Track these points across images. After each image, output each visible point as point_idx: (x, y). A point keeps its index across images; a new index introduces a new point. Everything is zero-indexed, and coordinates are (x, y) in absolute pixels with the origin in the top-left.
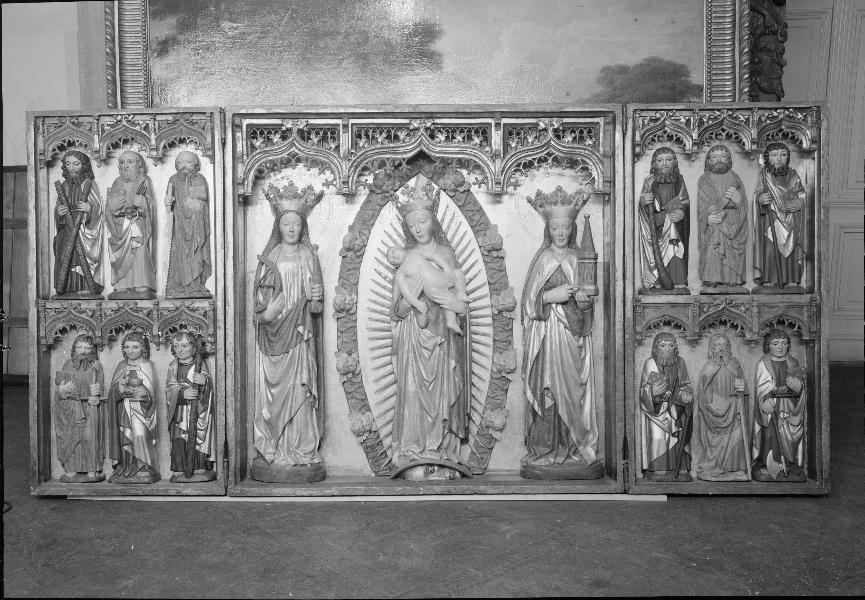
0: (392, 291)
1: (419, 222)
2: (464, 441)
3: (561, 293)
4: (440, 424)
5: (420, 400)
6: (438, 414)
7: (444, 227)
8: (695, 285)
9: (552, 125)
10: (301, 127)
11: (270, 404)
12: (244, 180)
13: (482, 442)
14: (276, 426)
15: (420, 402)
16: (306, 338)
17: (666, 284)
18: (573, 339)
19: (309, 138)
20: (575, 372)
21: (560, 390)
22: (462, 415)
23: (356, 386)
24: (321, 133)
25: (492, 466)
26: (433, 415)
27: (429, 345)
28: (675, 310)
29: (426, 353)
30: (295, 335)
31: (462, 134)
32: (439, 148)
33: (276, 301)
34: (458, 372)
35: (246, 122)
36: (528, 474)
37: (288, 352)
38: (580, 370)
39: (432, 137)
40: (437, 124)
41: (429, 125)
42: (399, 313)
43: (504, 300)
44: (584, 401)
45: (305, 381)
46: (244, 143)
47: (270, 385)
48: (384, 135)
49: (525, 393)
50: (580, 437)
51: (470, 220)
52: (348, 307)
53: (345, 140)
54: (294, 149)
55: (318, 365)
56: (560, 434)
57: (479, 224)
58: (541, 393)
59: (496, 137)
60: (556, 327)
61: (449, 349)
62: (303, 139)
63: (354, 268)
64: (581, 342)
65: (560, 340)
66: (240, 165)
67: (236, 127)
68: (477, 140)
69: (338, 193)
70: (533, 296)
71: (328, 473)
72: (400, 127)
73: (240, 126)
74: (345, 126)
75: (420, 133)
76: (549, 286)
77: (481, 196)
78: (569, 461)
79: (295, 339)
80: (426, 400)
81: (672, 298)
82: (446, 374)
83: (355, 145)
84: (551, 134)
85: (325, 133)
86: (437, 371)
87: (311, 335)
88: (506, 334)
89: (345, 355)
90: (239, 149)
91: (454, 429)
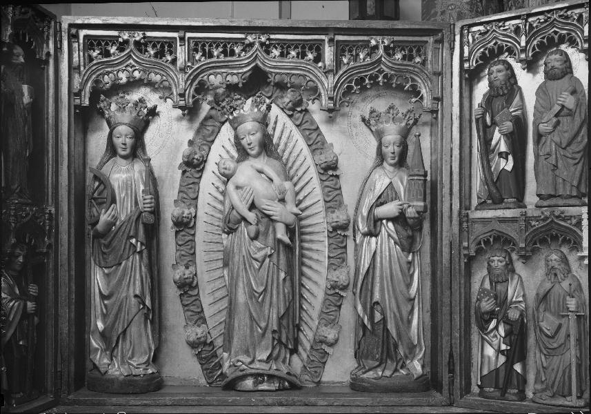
0: (222, 203)
1: (249, 134)
2: (294, 351)
3: (390, 209)
4: (269, 335)
5: (250, 310)
6: (267, 325)
7: (275, 141)
8: (531, 198)
9: (383, 42)
10: (138, 39)
11: (104, 316)
12: (80, 91)
13: (316, 356)
14: (111, 338)
15: (251, 314)
16: (138, 250)
17: (494, 198)
18: (402, 254)
19: (146, 51)
20: (403, 287)
21: (390, 305)
22: (291, 326)
23: (194, 298)
24: (159, 46)
25: (324, 379)
26: (263, 324)
27: (259, 255)
28: (503, 225)
29: (256, 265)
30: (128, 247)
31: (297, 50)
32: (273, 62)
33: (109, 212)
34: (288, 283)
35: (83, 33)
36: (357, 386)
37: (120, 264)
38: (409, 285)
39: (268, 52)
40: (272, 40)
41: (263, 39)
42: (231, 225)
43: (339, 217)
44: (412, 317)
45: (138, 292)
46: (81, 54)
47: (103, 297)
48: (220, 49)
49: (355, 308)
50: (407, 351)
51: (307, 139)
52: (185, 220)
53: (181, 53)
54: (131, 61)
55: (152, 278)
56: (388, 349)
57: (316, 143)
58: (372, 307)
59: (329, 53)
60: (386, 244)
61: (278, 260)
62: (140, 51)
63: (193, 183)
64: (410, 258)
65: (390, 255)
66: (77, 76)
67: (73, 37)
68: (310, 56)
69: (174, 107)
70: (365, 212)
71: (165, 383)
72: (236, 42)
73: (76, 36)
74: (182, 39)
75: (254, 49)
76: (380, 202)
77: (318, 117)
78: (397, 374)
79: (127, 250)
80: (255, 311)
81: (500, 213)
82: (275, 285)
83: (191, 58)
84: (381, 51)
85: (163, 46)
86: (267, 282)
87: (144, 247)
88: (340, 251)
89: (183, 268)
90: (76, 59)
91: (284, 340)
